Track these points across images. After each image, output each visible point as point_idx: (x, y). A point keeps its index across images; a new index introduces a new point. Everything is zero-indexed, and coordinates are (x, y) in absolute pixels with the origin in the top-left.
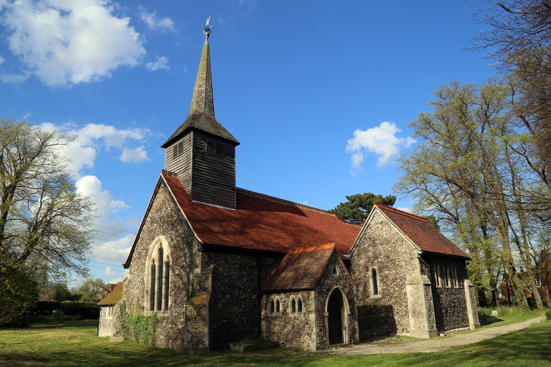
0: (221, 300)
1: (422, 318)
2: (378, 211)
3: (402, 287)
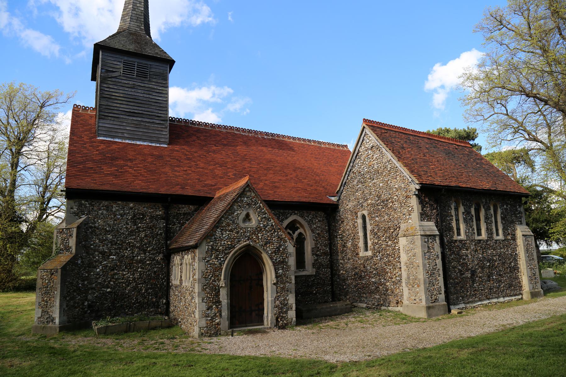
0: (102, 262)
1: (418, 286)
2: (368, 133)
3: (394, 238)
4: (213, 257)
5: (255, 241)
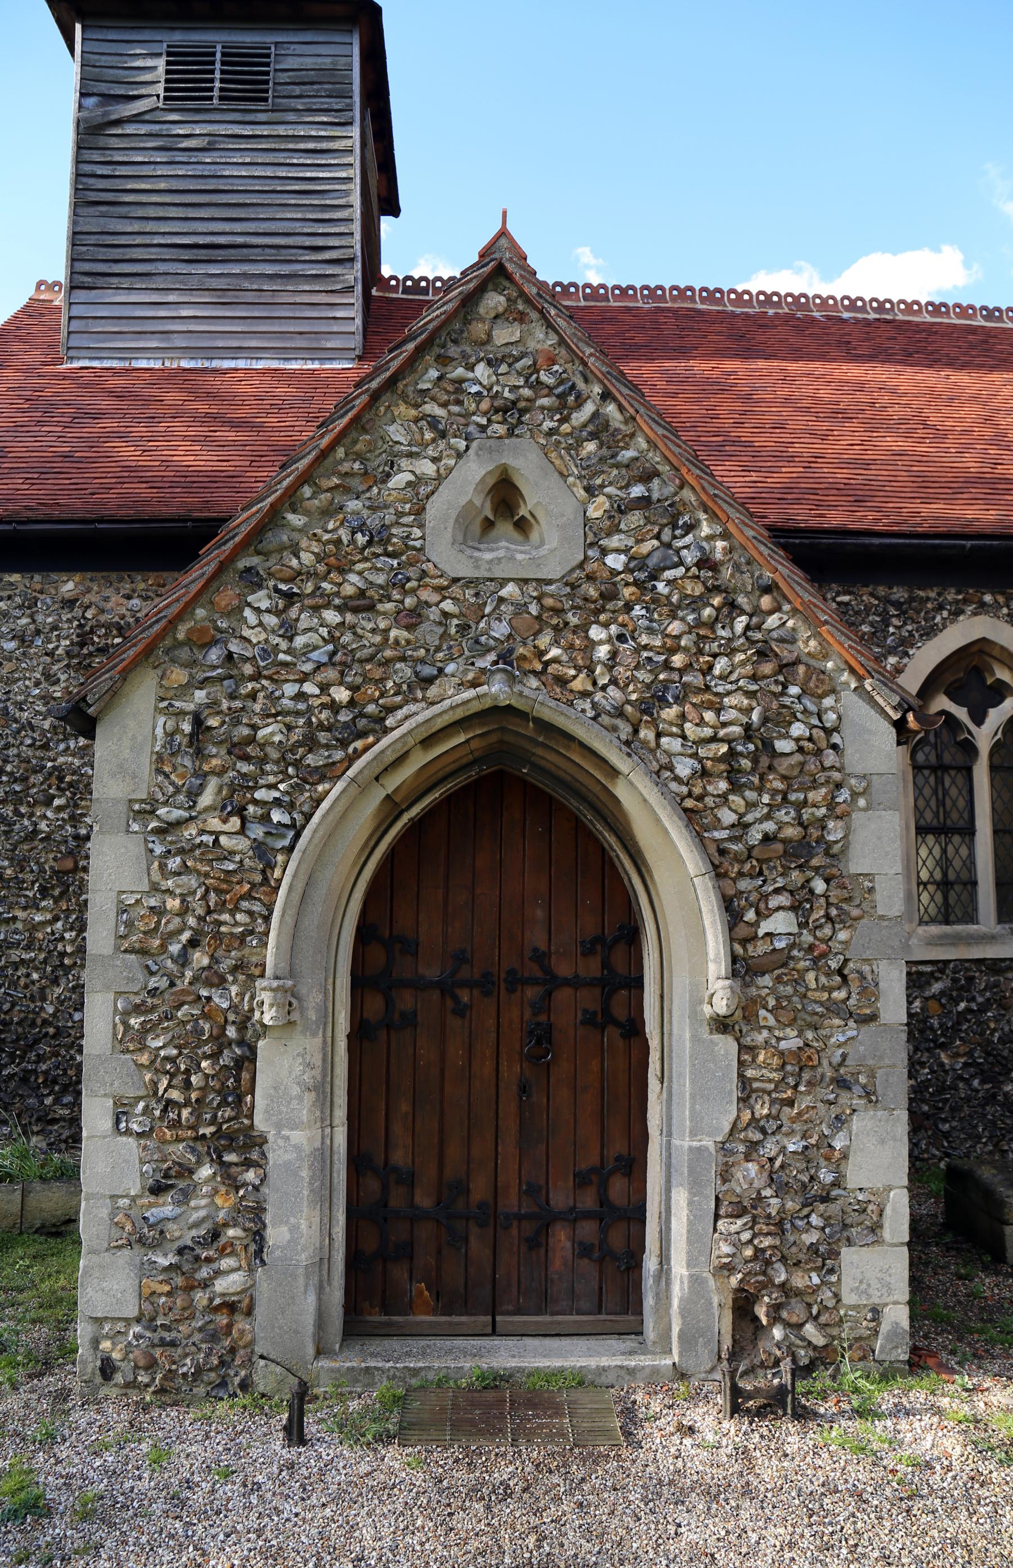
4: (206, 799)
5: (562, 681)
